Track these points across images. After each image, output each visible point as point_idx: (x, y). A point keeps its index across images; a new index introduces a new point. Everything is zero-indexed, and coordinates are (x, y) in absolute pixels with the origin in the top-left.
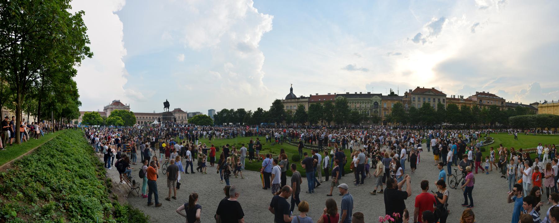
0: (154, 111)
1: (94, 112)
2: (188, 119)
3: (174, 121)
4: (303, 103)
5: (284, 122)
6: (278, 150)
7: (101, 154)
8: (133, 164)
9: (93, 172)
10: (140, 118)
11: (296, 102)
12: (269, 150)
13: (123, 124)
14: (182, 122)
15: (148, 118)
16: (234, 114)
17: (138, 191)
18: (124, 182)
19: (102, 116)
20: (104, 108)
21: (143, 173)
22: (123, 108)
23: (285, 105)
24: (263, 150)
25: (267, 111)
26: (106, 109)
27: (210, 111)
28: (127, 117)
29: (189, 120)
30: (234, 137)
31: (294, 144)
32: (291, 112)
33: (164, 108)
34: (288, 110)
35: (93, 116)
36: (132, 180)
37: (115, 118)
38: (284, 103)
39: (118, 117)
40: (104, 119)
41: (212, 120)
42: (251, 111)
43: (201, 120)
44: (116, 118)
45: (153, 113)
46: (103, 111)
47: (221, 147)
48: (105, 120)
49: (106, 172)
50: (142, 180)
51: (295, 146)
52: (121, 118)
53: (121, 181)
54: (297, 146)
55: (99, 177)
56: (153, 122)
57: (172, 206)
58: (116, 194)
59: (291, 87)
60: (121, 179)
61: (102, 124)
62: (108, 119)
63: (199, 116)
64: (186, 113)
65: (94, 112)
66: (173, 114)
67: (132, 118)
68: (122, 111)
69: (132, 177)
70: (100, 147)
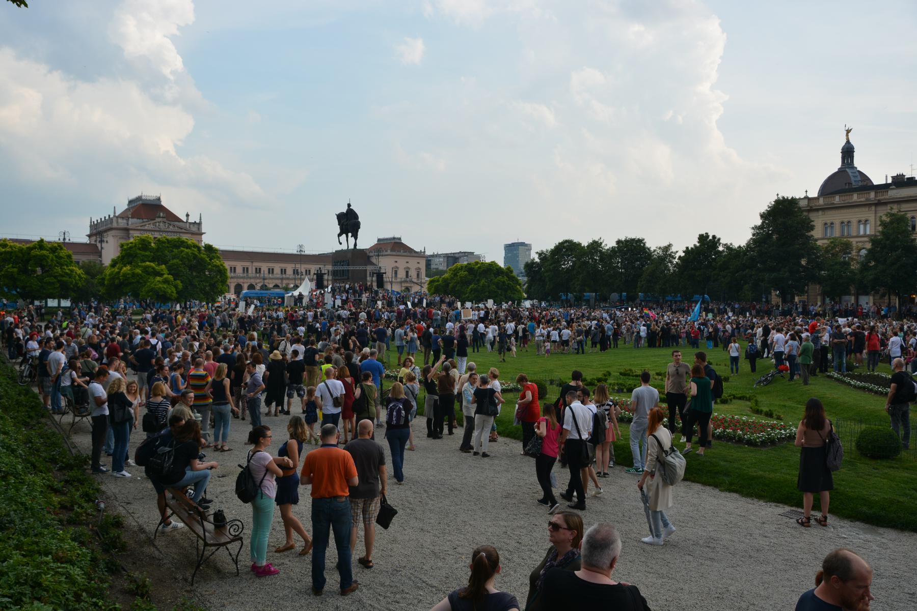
0: (301, 246)
1: (42, 241)
2: (428, 279)
3: (375, 284)
4: (905, 207)
5: (815, 289)
6: (788, 403)
7: (77, 419)
8: (216, 449)
9: (34, 498)
10: (245, 270)
11: (870, 205)
12: (748, 403)
13: (175, 295)
14: (408, 289)
15: (277, 270)
16: (601, 260)
17: (234, 552)
18: (177, 523)
19: (83, 259)
20: (91, 226)
21: (254, 482)
22: (176, 229)
23: (818, 221)
24: (724, 402)
25: (736, 245)
26: (99, 231)
27: (512, 249)
28: (191, 268)
29: (431, 282)
30: (604, 348)
31: (863, 384)
32: (847, 247)
33: (339, 235)
34: (834, 242)
35: (41, 261)
36: (212, 511)
37: (138, 271)
38: (811, 210)
39: (152, 264)
40: (92, 270)
41: (517, 280)
42: (670, 245)
43: (479, 281)
44: (146, 270)
45: (295, 252)
46: (86, 240)
47: (552, 382)
48: (93, 276)
49: (98, 490)
50: (248, 508)
51: (866, 395)
52: (166, 272)
53: (165, 521)
54: (881, 393)
55: (64, 516)
56: (296, 287)
57: (369, 602)
58: (141, 573)
59: (848, 142)
60: (163, 512)
61: (80, 295)
62: (108, 272)
63: (470, 269)
64: (420, 255)
65: (41, 244)
66: (374, 260)
67: (210, 271)
68: (168, 241)
69: (210, 501)
70: (69, 392)
